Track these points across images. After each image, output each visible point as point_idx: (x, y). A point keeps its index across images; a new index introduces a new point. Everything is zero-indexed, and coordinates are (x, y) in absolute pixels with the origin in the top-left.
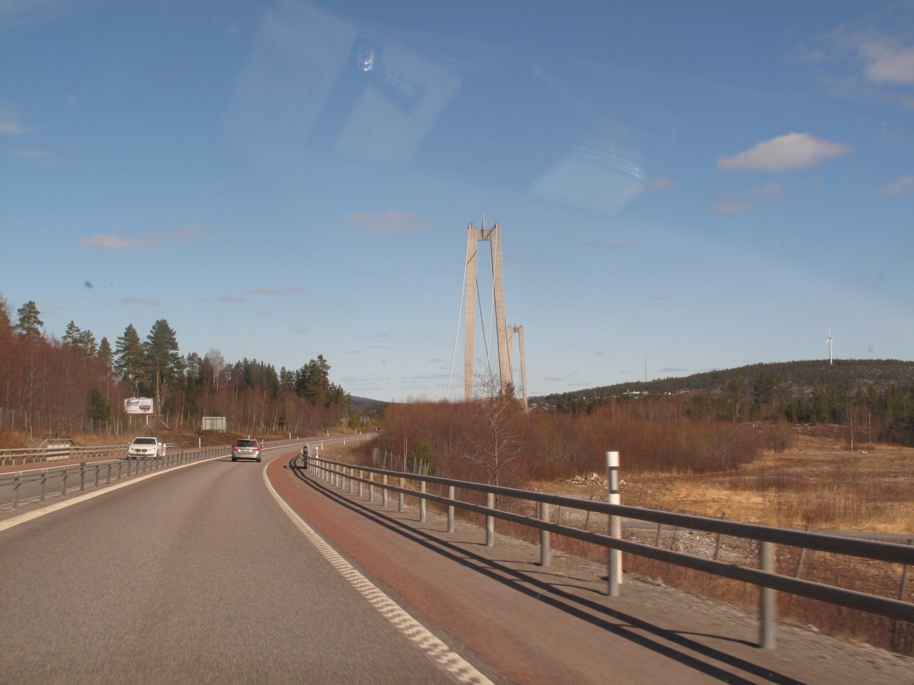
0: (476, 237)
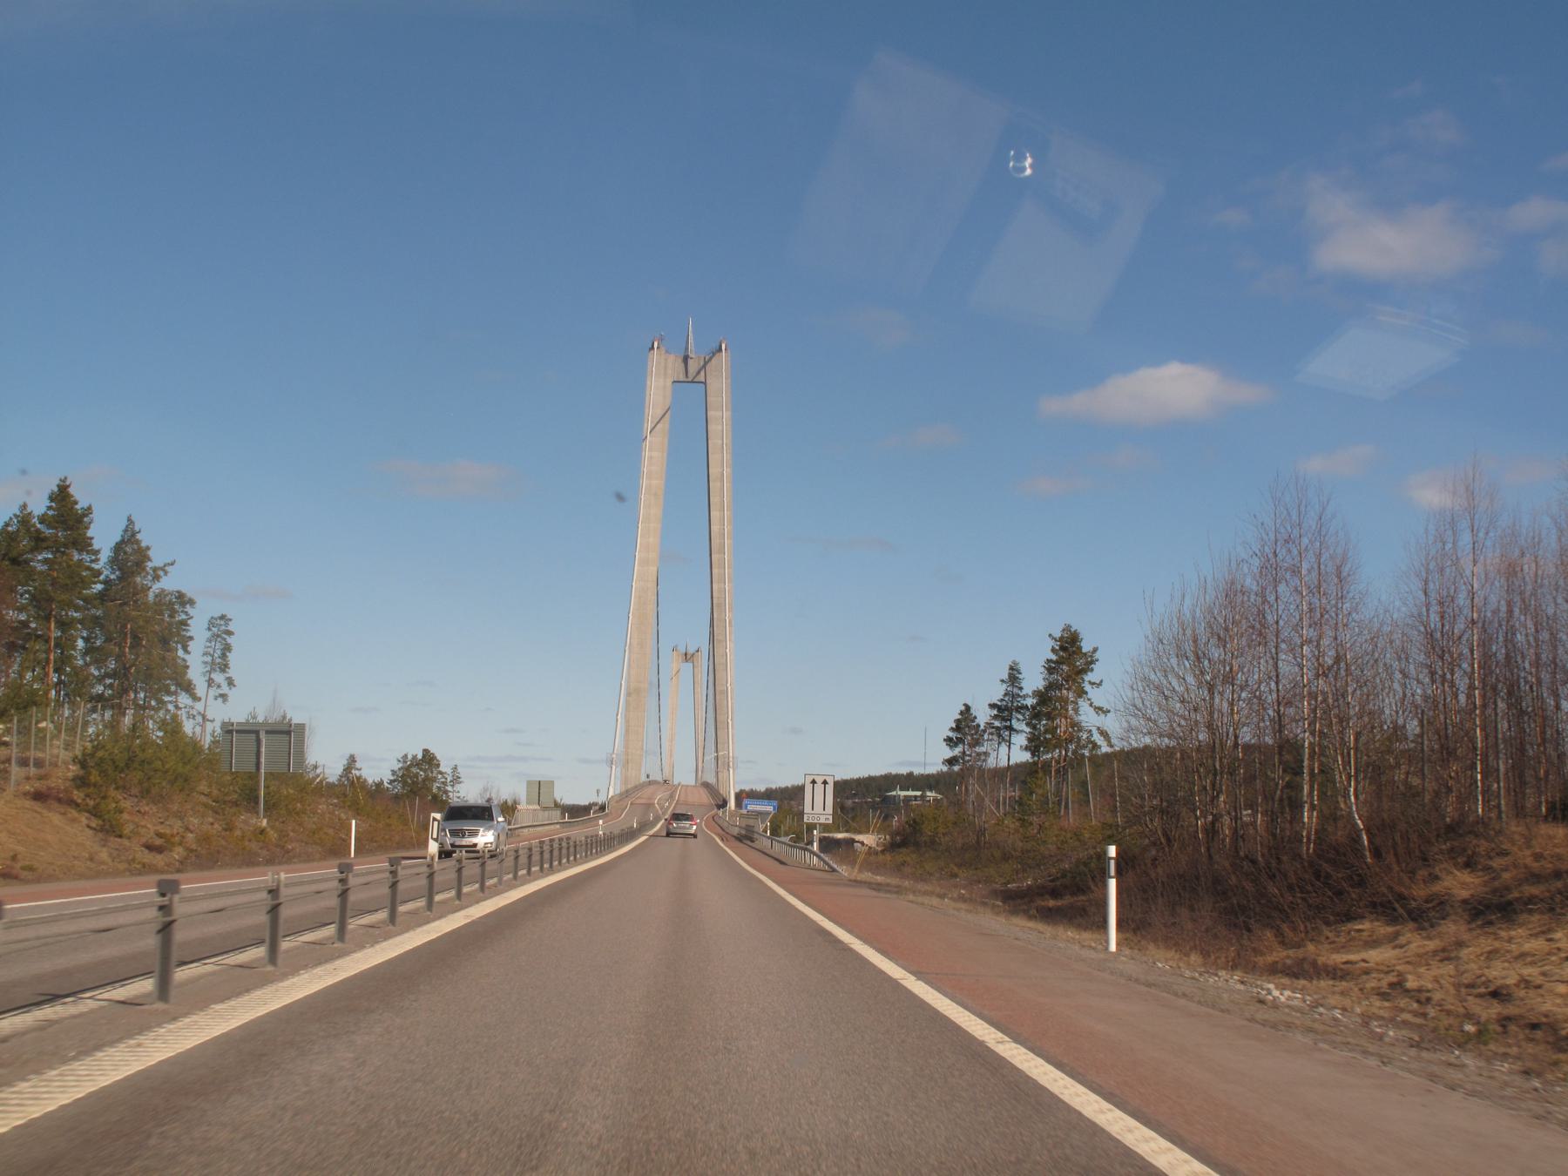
0: (670, 372)
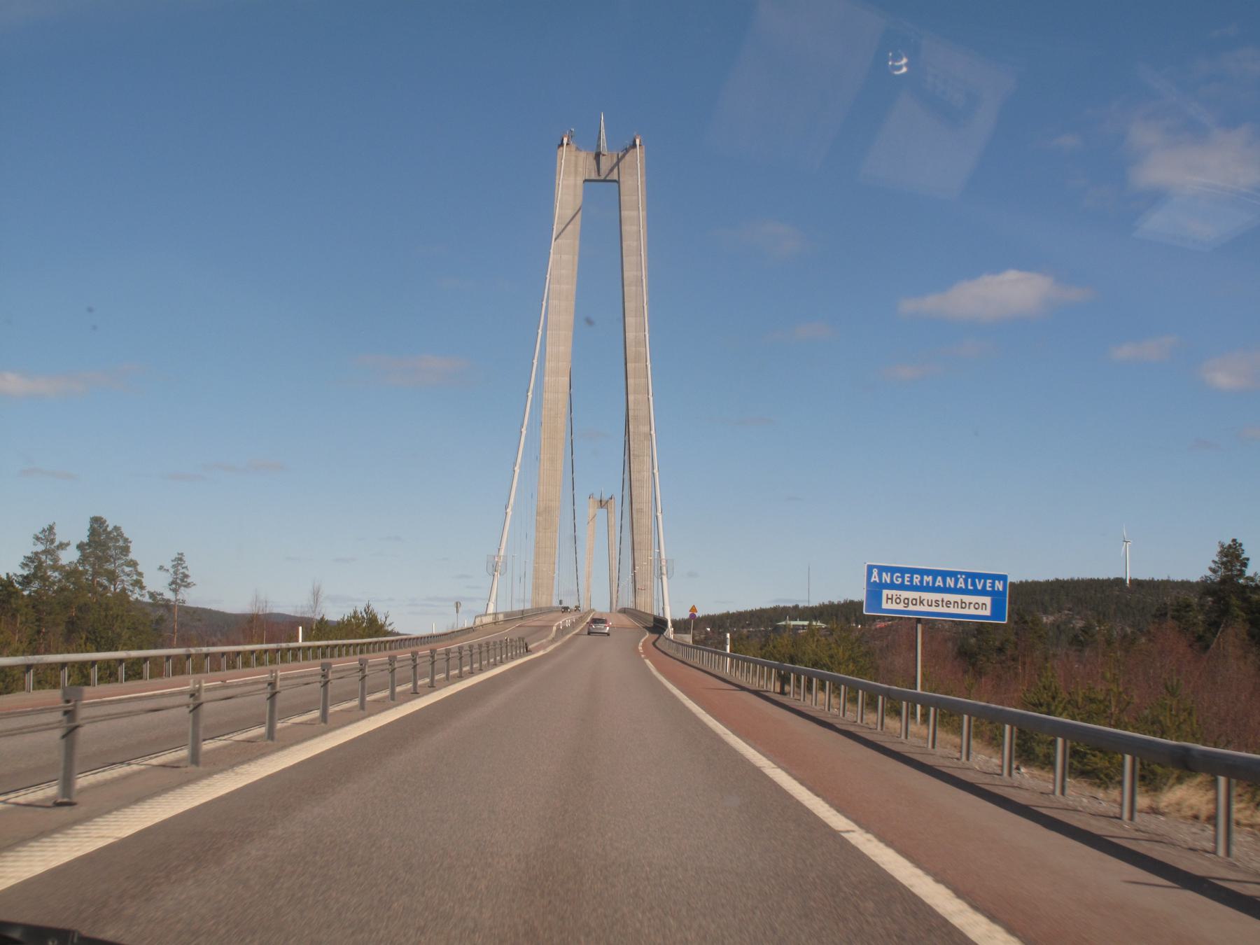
0: (581, 169)
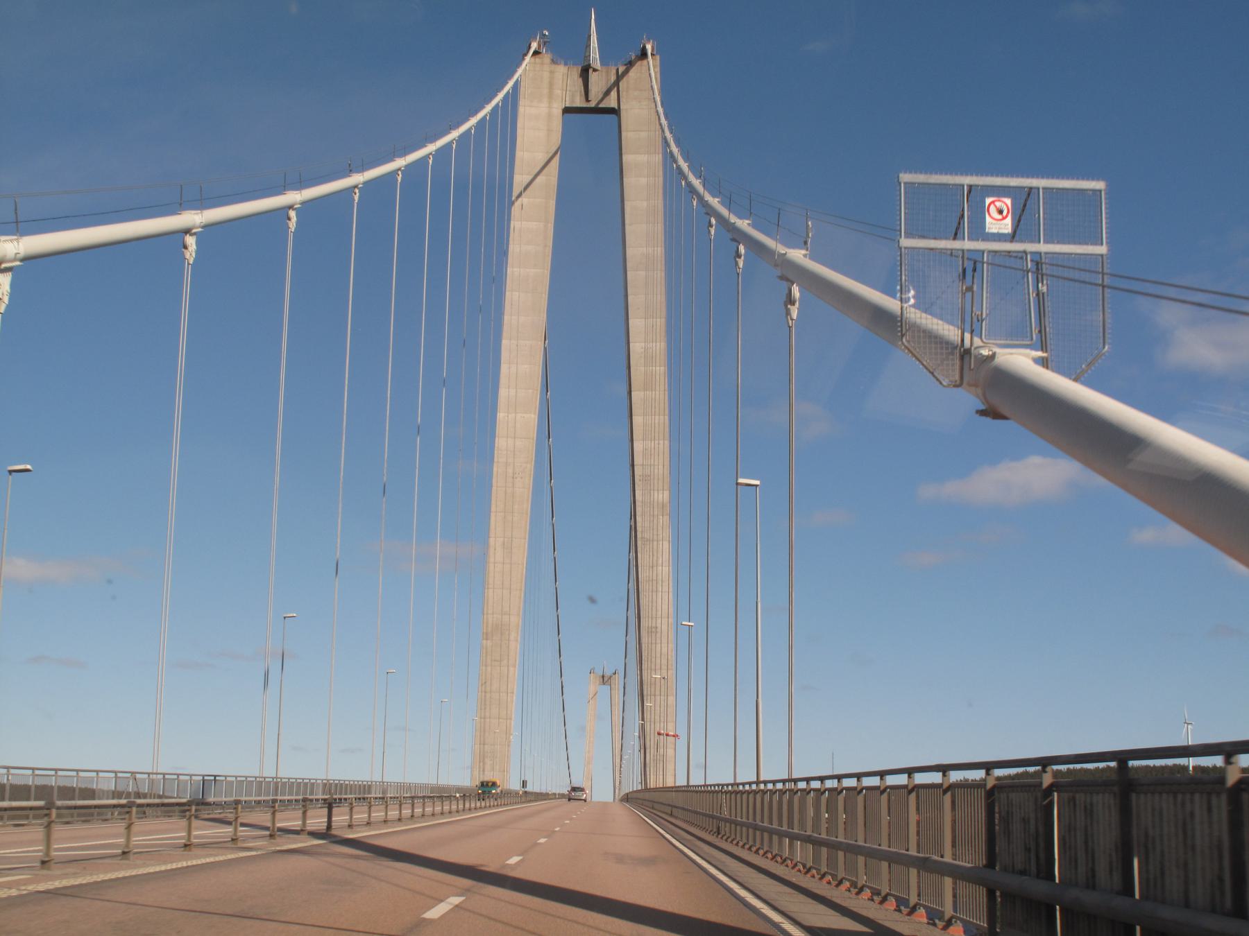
0: (558, 92)
